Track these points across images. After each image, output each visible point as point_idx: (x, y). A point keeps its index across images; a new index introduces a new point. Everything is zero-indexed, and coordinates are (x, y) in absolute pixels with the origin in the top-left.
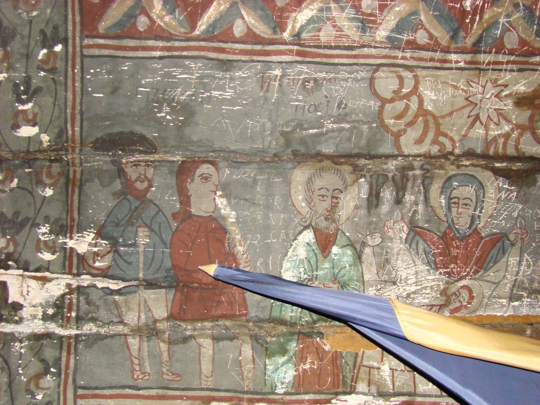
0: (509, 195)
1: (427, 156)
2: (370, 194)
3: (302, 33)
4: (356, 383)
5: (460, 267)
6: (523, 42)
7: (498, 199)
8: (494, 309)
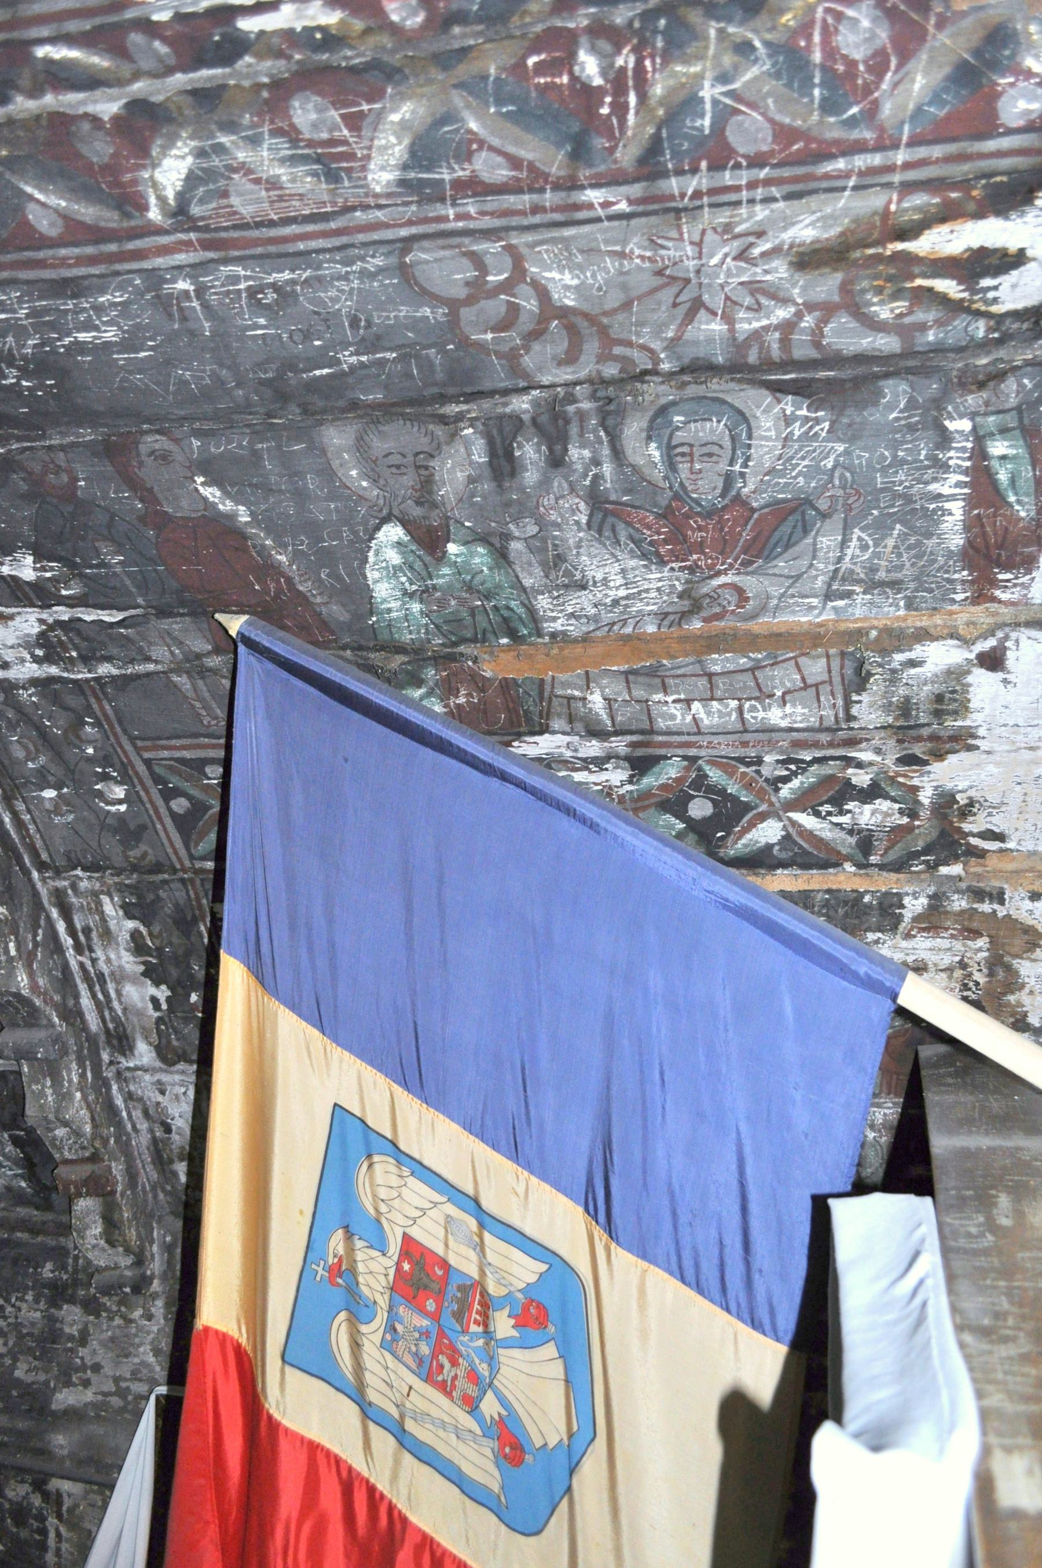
0: (811, 428)
1: (597, 382)
2: (492, 453)
3: (189, 205)
4: (548, 719)
5: (711, 558)
6: (784, 134)
7: (786, 439)
8: (794, 612)
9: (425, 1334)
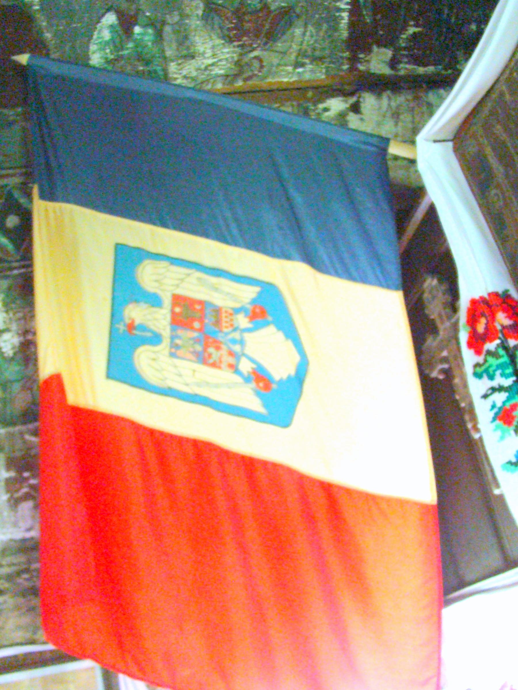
9: (197, 340)
